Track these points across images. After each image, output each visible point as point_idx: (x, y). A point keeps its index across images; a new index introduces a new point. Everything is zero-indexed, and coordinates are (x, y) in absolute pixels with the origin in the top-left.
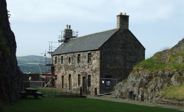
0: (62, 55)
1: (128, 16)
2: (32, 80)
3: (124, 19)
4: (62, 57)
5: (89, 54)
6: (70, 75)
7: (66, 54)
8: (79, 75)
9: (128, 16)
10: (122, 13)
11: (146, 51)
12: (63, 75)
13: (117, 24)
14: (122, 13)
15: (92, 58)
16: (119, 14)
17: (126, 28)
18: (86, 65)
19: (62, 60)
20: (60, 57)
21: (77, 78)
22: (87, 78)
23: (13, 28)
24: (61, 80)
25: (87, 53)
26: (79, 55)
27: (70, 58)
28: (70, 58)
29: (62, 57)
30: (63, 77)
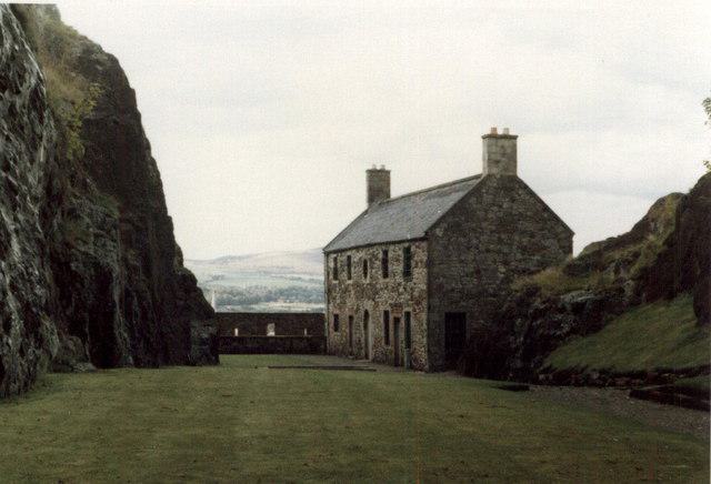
0: (349, 253)
1: (388, 172)
2: (308, 333)
3: (501, 147)
4: (349, 257)
5: (407, 251)
6: (366, 313)
7: (357, 248)
8: (386, 313)
9: (388, 172)
10: (507, 129)
11: (575, 239)
12: (453, 309)
13: (484, 160)
14: (507, 129)
15: (413, 264)
16: (488, 132)
17: (511, 174)
18: (399, 284)
19: (349, 265)
20: (344, 258)
21: (382, 320)
22: (403, 321)
23: (140, 108)
24: (348, 331)
25: (401, 246)
26: (386, 253)
27: (365, 262)
28: (365, 262)
29: (349, 257)
30: (351, 318)
